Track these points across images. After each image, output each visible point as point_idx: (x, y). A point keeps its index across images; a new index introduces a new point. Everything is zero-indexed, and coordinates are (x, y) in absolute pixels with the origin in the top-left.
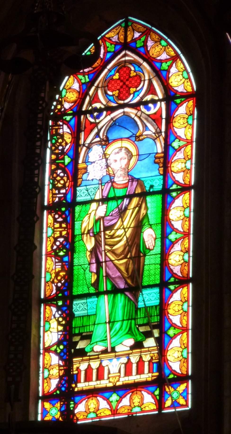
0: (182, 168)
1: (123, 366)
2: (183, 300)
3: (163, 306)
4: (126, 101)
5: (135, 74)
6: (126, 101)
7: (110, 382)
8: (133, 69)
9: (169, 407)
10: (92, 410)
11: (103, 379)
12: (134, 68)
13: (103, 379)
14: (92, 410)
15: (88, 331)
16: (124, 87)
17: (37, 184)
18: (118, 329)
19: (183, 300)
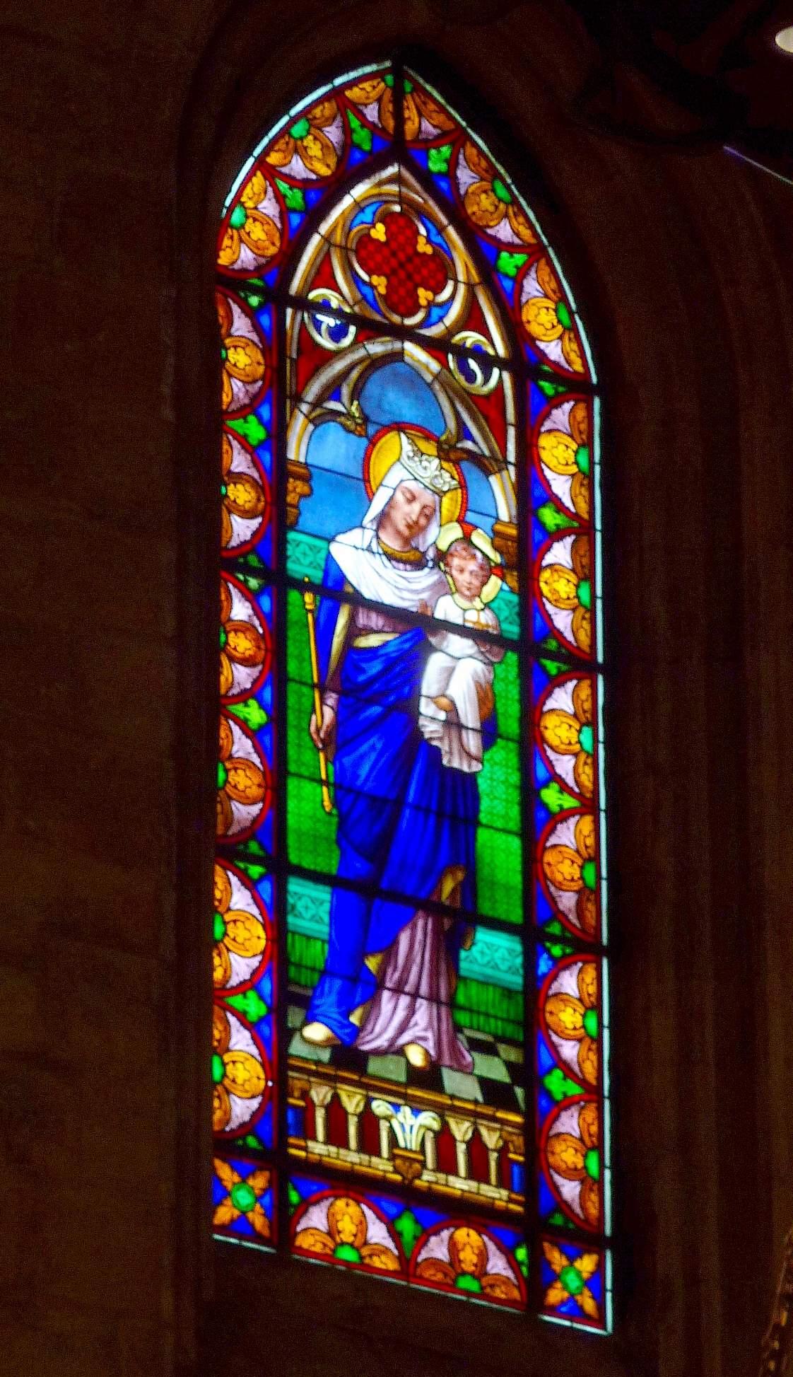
0: (339, 1232)
1: (430, 1135)
2: (365, 1251)
3: (534, 992)
4: (409, 322)
5: (423, 302)
6: (409, 322)
7: (396, 1171)
8: (423, 231)
9: (223, 1229)
10: (250, 225)
11: (472, 778)
12: (428, 230)
13: (472, 778)
14: (250, 225)
15: (302, 460)
16: (410, 267)
17: (273, 941)
18: (389, 1014)
19: (365, 1251)
